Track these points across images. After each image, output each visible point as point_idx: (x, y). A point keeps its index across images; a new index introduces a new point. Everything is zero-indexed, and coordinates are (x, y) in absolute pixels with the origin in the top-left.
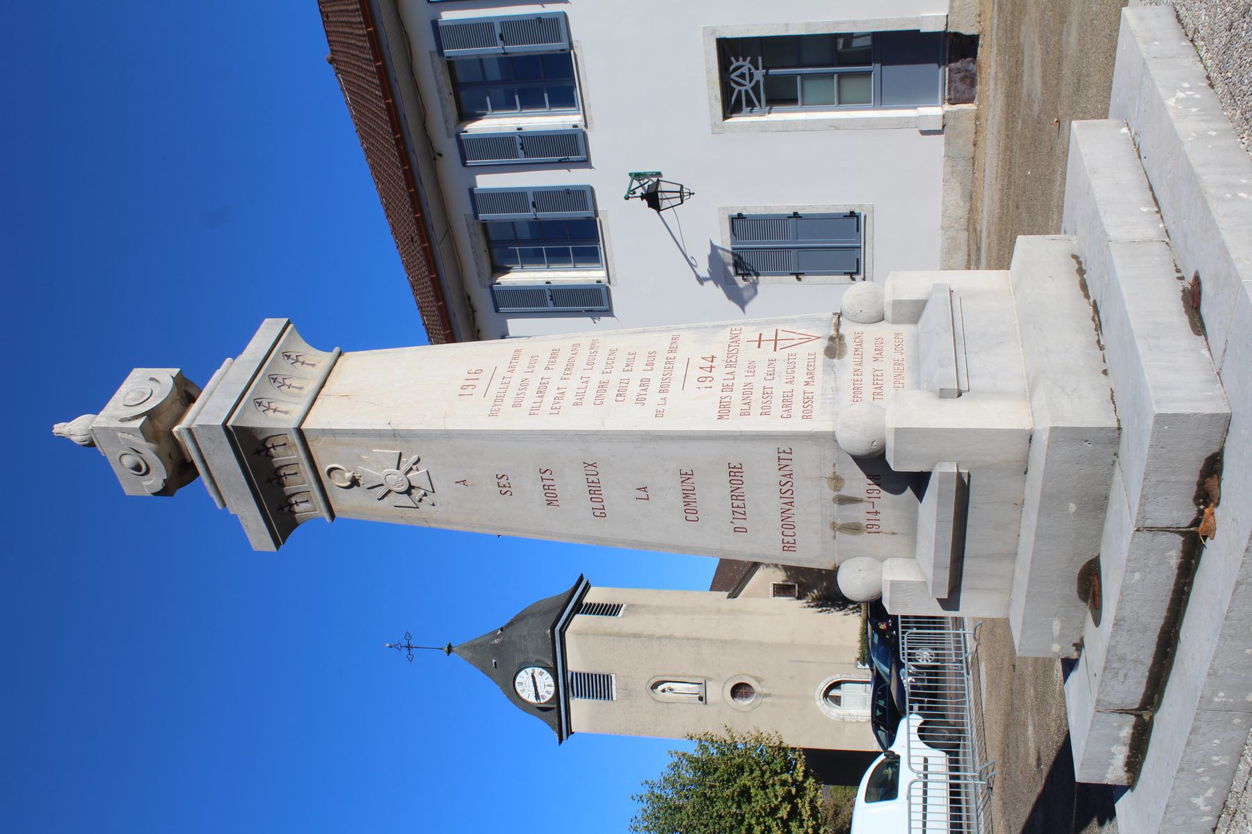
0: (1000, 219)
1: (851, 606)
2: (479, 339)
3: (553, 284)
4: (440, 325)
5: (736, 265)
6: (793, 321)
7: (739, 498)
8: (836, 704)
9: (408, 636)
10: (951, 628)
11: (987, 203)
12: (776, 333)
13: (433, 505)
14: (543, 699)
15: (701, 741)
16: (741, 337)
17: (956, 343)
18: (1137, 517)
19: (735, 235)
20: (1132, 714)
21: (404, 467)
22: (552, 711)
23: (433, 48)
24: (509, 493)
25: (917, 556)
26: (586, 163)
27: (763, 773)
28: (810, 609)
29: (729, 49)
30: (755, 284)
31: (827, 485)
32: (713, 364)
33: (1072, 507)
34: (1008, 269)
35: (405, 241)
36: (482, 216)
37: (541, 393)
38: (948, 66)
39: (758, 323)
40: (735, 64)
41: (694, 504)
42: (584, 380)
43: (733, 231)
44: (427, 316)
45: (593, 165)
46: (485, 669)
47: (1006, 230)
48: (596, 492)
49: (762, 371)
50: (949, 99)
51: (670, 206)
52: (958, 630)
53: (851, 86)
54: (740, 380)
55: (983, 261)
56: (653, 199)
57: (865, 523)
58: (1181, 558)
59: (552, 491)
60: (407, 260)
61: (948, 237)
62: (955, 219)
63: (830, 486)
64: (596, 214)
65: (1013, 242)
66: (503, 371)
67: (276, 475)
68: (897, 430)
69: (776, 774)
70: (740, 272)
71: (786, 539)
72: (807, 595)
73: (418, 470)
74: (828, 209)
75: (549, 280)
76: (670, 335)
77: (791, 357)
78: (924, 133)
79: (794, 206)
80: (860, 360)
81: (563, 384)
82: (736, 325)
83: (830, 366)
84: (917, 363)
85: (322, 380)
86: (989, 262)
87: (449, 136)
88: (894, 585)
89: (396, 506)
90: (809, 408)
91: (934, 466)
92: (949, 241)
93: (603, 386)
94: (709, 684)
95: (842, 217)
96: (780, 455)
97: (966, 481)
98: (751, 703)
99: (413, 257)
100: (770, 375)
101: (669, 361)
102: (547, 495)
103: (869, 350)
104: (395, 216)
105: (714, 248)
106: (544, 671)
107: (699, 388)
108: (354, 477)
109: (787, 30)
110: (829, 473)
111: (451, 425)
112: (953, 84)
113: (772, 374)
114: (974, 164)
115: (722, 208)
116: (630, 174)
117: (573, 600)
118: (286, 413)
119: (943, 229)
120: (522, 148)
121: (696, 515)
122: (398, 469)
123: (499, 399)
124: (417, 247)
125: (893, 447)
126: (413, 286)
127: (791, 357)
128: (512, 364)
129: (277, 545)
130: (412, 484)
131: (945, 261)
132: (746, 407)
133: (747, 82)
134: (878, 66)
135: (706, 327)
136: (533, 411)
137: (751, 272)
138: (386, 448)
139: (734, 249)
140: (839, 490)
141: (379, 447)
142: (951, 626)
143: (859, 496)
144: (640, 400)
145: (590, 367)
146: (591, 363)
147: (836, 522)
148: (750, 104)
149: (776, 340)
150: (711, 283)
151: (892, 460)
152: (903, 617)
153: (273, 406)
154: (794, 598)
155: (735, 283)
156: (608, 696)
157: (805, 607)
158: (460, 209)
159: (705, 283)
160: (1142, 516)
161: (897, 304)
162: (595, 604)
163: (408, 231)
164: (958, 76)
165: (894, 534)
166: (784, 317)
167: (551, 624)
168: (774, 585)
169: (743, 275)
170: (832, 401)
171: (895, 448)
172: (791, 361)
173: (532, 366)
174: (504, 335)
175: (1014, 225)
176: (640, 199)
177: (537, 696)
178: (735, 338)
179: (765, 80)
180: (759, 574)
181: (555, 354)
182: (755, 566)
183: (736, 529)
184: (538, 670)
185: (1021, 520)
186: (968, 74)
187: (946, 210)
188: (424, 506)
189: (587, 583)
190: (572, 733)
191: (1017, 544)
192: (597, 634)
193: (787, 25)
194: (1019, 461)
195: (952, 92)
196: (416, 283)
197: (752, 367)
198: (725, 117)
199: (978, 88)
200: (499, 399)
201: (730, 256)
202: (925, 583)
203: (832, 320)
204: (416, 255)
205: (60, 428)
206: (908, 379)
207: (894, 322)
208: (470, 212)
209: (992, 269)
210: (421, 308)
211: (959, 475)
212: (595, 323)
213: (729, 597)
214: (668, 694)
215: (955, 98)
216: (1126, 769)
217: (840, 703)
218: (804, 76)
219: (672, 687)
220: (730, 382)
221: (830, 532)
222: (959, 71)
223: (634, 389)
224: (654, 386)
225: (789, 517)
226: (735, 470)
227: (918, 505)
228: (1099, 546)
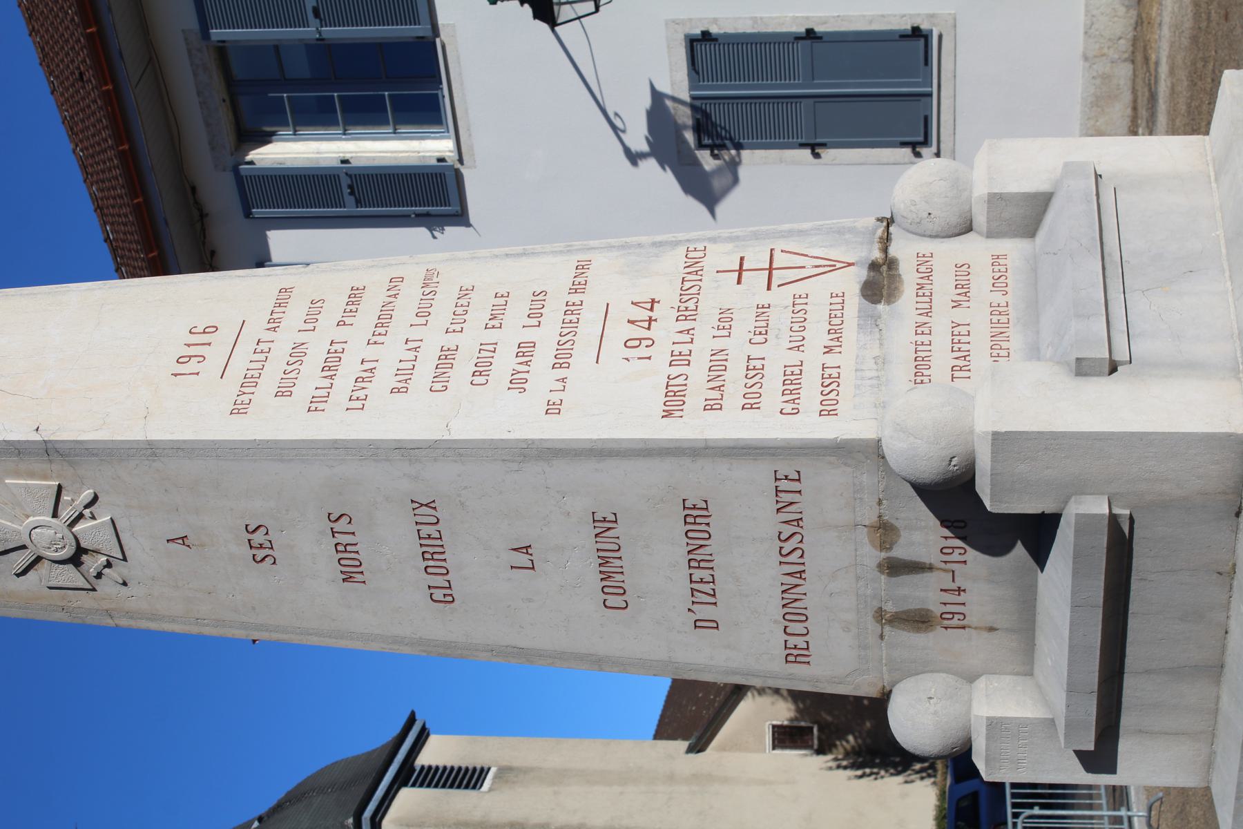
0: (1194, 39)
1: (918, 766)
2: (213, 268)
3: (354, 163)
4: (137, 242)
5: (698, 129)
6: (801, 233)
7: (702, 564)
10: (1105, 806)
11: (1170, 9)
12: (772, 256)
13: (125, 584)
16: (705, 263)
17: (1107, 273)
19: (698, 73)
21: (66, 513)
24: (269, 560)
25: (1037, 671)
28: (841, 772)
30: (734, 165)
31: (866, 540)
32: (654, 315)
34: (1207, 133)
35: (67, 78)
36: (217, 33)
37: (330, 368)
39: (737, 238)
41: (618, 577)
42: (411, 345)
44: (112, 224)
45: (472, 221)
47: (1205, 60)
48: (436, 556)
49: (744, 324)
51: (576, 17)
52: (1119, 810)
54: (704, 344)
55: (1162, 119)
57: (937, 610)
59: (353, 556)
60: (72, 117)
61: (1095, 74)
62: (1110, 40)
63: (872, 542)
65: (1216, 82)
66: (257, 328)
68: (996, 436)
70: (706, 141)
71: (792, 641)
72: (835, 746)
73: (93, 518)
74: (871, 22)
75: (348, 156)
76: (573, 261)
77: (798, 301)
79: (807, 18)
80: (927, 306)
81: (371, 352)
82: (697, 240)
84: (1034, 308)
86: (1172, 119)
88: (995, 725)
89: (50, 588)
90: (832, 396)
91: (1066, 502)
92: (1098, 81)
93: (446, 357)
95: (897, 38)
96: (778, 483)
97: (1126, 530)
99: (83, 110)
100: (760, 333)
101: (572, 310)
102: (343, 562)
103: (944, 286)
104: (47, 30)
105: (657, 97)
107: (627, 359)
110: (870, 516)
111: (159, 431)
113: (762, 332)
119: (1086, 58)
120: (352, 193)
121: (624, 598)
122: (55, 515)
123: (250, 381)
125: (989, 468)
126: (84, 167)
127: (798, 301)
128: (275, 316)
130: (83, 545)
131: (1089, 119)
132: (716, 394)
135: (640, 245)
136: (316, 405)
137: (728, 143)
138: (32, 475)
139: (693, 98)
140: (890, 549)
141: (17, 474)
142: (1104, 801)
143: (925, 560)
144: (518, 383)
145: (423, 320)
146: (423, 313)
147: (884, 608)
149: (771, 269)
150: (651, 165)
151: (988, 491)
152: (1014, 786)
154: (812, 752)
155: (696, 163)
157: (831, 768)
159: (640, 163)
161: (996, 200)
162: (437, 768)
163: (72, 61)
166: (787, 227)
168: (774, 727)
169: (711, 148)
170: (875, 382)
171: (992, 470)
172: (798, 308)
173: (312, 319)
174: (262, 260)
175: (1220, 52)
178: (694, 267)
180: (746, 708)
181: (355, 296)
182: (737, 692)
183: (699, 624)
185: (1229, 602)
187: (1092, 24)
188: (105, 587)
191: (1224, 648)
194: (1225, 493)
196: (90, 161)
197: (725, 320)
200: (250, 381)
201: (688, 111)
202: (1053, 720)
204: (89, 107)
206: (1016, 340)
207: (990, 235)
208: (192, 23)
209: (1179, 134)
210: (101, 209)
211: (1113, 519)
212: (434, 237)
213: (690, 750)
220: (685, 349)
221: (872, 627)
223: (505, 362)
224: (544, 356)
225: (796, 600)
226: (695, 513)
227: (1036, 575)
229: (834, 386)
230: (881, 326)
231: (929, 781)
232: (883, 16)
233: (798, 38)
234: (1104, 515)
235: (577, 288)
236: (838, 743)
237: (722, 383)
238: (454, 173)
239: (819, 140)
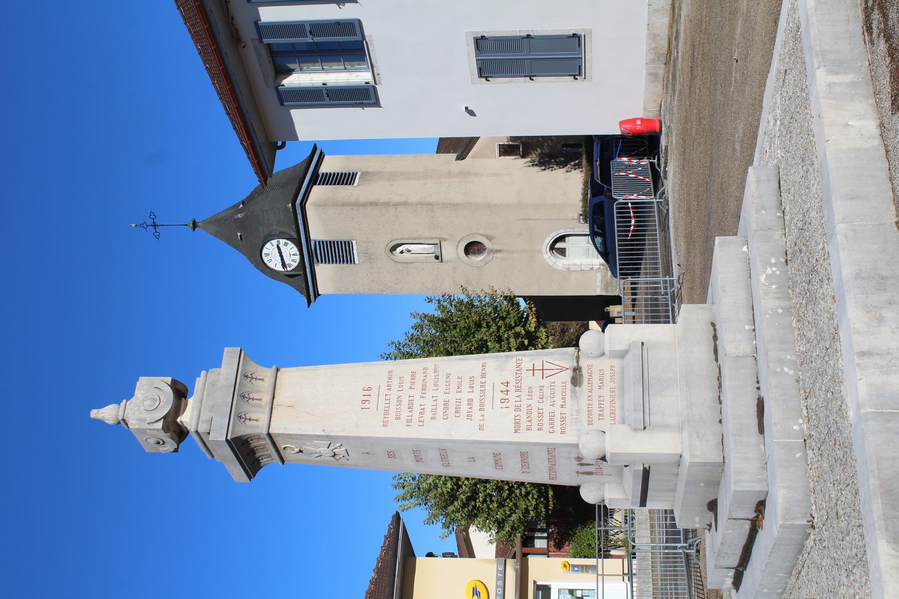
3: (329, 85)
8: (562, 255)
9: (152, 215)
12: (543, 363)
14: (290, 267)
15: (439, 303)
16: (523, 366)
22: (299, 277)
27: (499, 328)
29: (480, 43)
32: (508, 388)
33: (702, 484)
36: (266, 41)
46: (231, 242)
52: (666, 277)
54: (524, 403)
69: (511, 328)
72: (531, 153)
83: (574, 392)
85: (273, 394)
87: (268, 87)
94: (444, 244)
98: (484, 258)
101: (483, 385)
106: (288, 242)
117: (309, 171)
118: (257, 420)
120: (328, 96)
123: (386, 413)
124: (238, 119)
129: (250, 478)
138: (322, 441)
153: (248, 416)
156: (351, 260)
157: (529, 166)
158: (248, 34)
167: (291, 197)
170: (576, 420)
177: (284, 265)
184: (282, 241)
189: (321, 153)
190: (319, 295)
192: (336, 205)
203: (574, 354)
205: (94, 414)
208: (256, 36)
212: (340, 8)
213: (458, 158)
214: (406, 255)
217: (565, 254)
219: (410, 248)
223: (464, 407)
228: (717, 491)
229: (564, 422)
230: (578, 397)
231: (578, 171)
233: (523, 38)
234: (641, 470)
235: (483, 376)
236: (532, 152)
237: (531, 419)
238: (358, 22)
239: (533, 74)
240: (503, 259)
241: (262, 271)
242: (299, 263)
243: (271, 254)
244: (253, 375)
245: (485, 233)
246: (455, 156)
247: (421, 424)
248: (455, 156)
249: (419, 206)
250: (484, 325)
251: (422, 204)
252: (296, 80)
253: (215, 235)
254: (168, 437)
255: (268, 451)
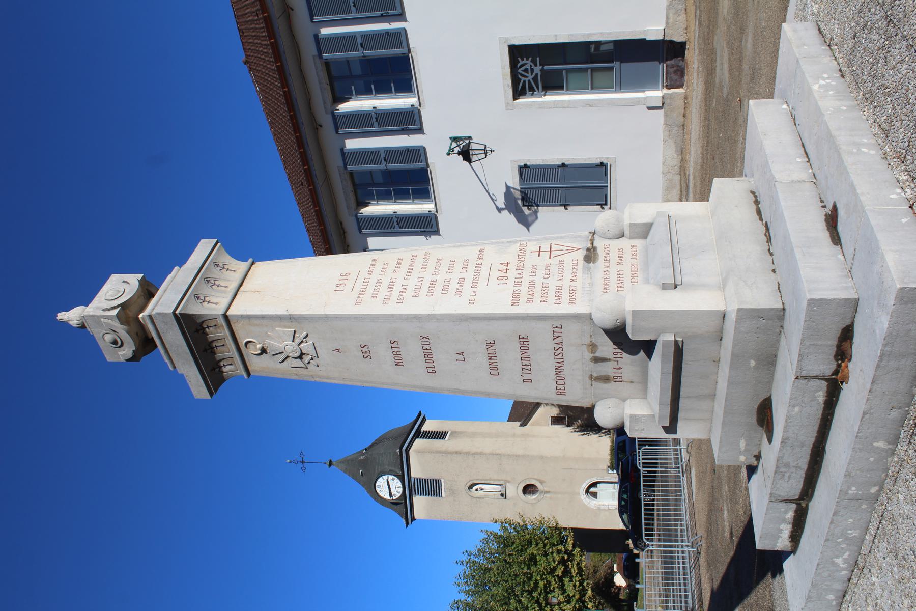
3: (398, 213)
5: (523, 199)
12: (551, 246)
14: (395, 496)
18: (796, 369)
20: (794, 503)
21: (297, 341)
23: (315, 52)
26: (420, 130)
27: (545, 545)
29: (517, 53)
30: (536, 212)
33: (753, 363)
36: (350, 167)
38: (665, 63)
40: (521, 63)
43: (521, 176)
45: (408, 19)
46: (355, 477)
50: (667, 86)
53: (600, 77)
56: (466, 155)
58: (826, 397)
64: (428, 165)
67: (210, 346)
69: (554, 545)
72: (574, 424)
78: (650, 108)
79: (562, 159)
83: (588, 268)
87: (326, 113)
94: (508, 485)
98: (537, 497)
101: (478, 266)
106: (395, 477)
108: (263, 347)
109: (556, 39)
110: (587, 341)
112: (669, 75)
114: (683, 130)
115: (513, 160)
116: (451, 138)
118: (216, 304)
122: (293, 341)
129: (211, 394)
133: (529, 75)
134: (618, 63)
139: (521, 188)
140: (595, 353)
148: (532, 89)
150: (506, 212)
155: (522, 212)
156: (439, 494)
157: (572, 432)
160: (800, 368)
164: (672, 70)
165: (632, 382)
167: (399, 445)
176: (457, 155)
179: (542, 72)
183: (525, 381)
184: (391, 477)
186: (679, 68)
189: (424, 417)
193: (556, 36)
195: (668, 81)
198: (515, 98)
199: (686, 78)
201: (519, 193)
205: (62, 316)
212: (427, 239)
213: (521, 425)
214: (480, 492)
215: (670, 85)
216: (790, 540)
218: (568, 70)
222: (673, 66)
228: (770, 389)
229: (574, 294)
231: (608, 436)
232: (590, 158)
233: (559, 166)
234: (673, 340)
239: (567, 203)
240: (551, 498)
241: (375, 499)
242: (402, 494)
243: (381, 487)
244: (225, 266)
245: (539, 478)
246: (519, 423)
247: (401, 301)
248: (519, 423)
249: (490, 456)
250: (534, 543)
251: (493, 454)
252: (355, 105)
253: (344, 472)
254: (123, 329)
255: (229, 352)
